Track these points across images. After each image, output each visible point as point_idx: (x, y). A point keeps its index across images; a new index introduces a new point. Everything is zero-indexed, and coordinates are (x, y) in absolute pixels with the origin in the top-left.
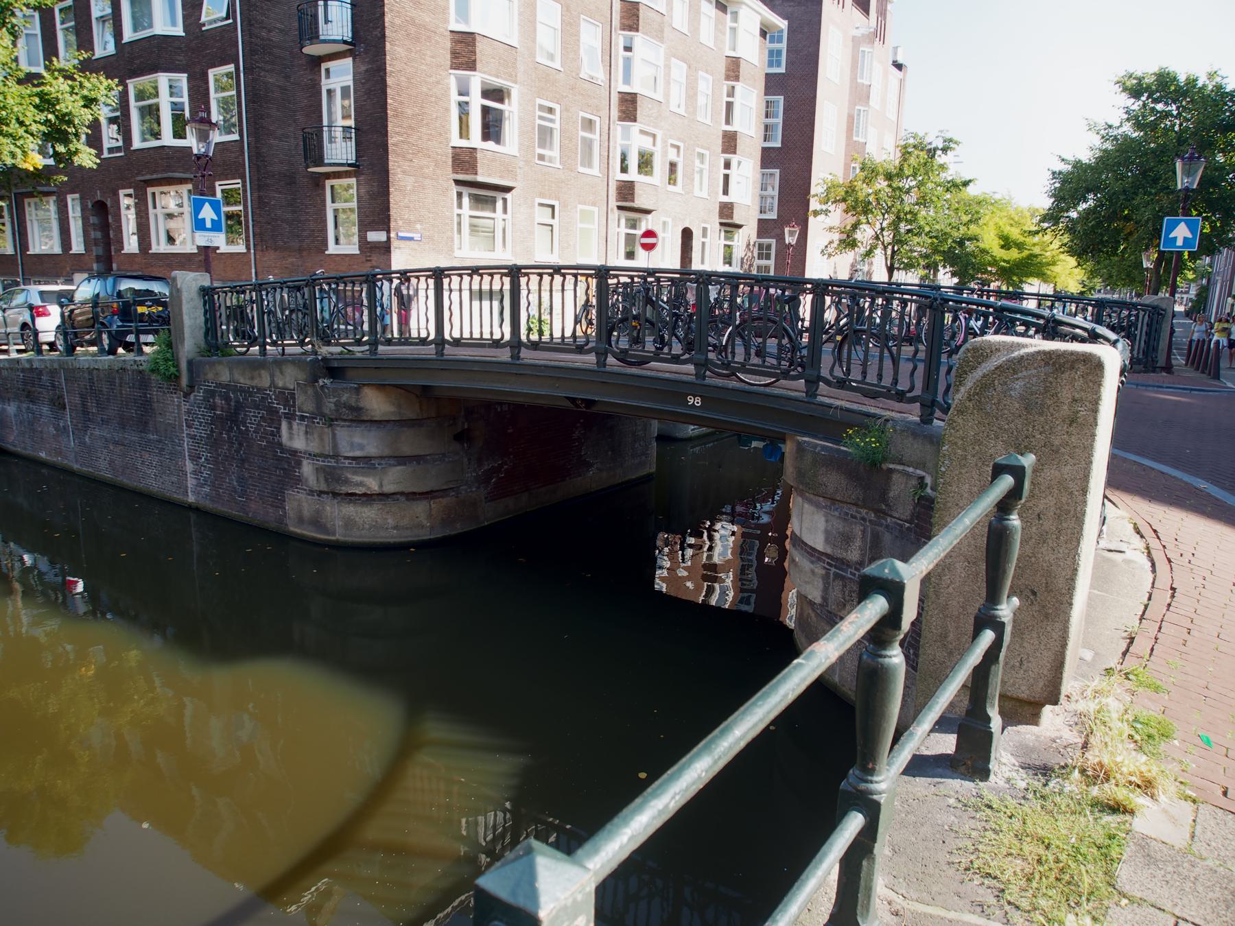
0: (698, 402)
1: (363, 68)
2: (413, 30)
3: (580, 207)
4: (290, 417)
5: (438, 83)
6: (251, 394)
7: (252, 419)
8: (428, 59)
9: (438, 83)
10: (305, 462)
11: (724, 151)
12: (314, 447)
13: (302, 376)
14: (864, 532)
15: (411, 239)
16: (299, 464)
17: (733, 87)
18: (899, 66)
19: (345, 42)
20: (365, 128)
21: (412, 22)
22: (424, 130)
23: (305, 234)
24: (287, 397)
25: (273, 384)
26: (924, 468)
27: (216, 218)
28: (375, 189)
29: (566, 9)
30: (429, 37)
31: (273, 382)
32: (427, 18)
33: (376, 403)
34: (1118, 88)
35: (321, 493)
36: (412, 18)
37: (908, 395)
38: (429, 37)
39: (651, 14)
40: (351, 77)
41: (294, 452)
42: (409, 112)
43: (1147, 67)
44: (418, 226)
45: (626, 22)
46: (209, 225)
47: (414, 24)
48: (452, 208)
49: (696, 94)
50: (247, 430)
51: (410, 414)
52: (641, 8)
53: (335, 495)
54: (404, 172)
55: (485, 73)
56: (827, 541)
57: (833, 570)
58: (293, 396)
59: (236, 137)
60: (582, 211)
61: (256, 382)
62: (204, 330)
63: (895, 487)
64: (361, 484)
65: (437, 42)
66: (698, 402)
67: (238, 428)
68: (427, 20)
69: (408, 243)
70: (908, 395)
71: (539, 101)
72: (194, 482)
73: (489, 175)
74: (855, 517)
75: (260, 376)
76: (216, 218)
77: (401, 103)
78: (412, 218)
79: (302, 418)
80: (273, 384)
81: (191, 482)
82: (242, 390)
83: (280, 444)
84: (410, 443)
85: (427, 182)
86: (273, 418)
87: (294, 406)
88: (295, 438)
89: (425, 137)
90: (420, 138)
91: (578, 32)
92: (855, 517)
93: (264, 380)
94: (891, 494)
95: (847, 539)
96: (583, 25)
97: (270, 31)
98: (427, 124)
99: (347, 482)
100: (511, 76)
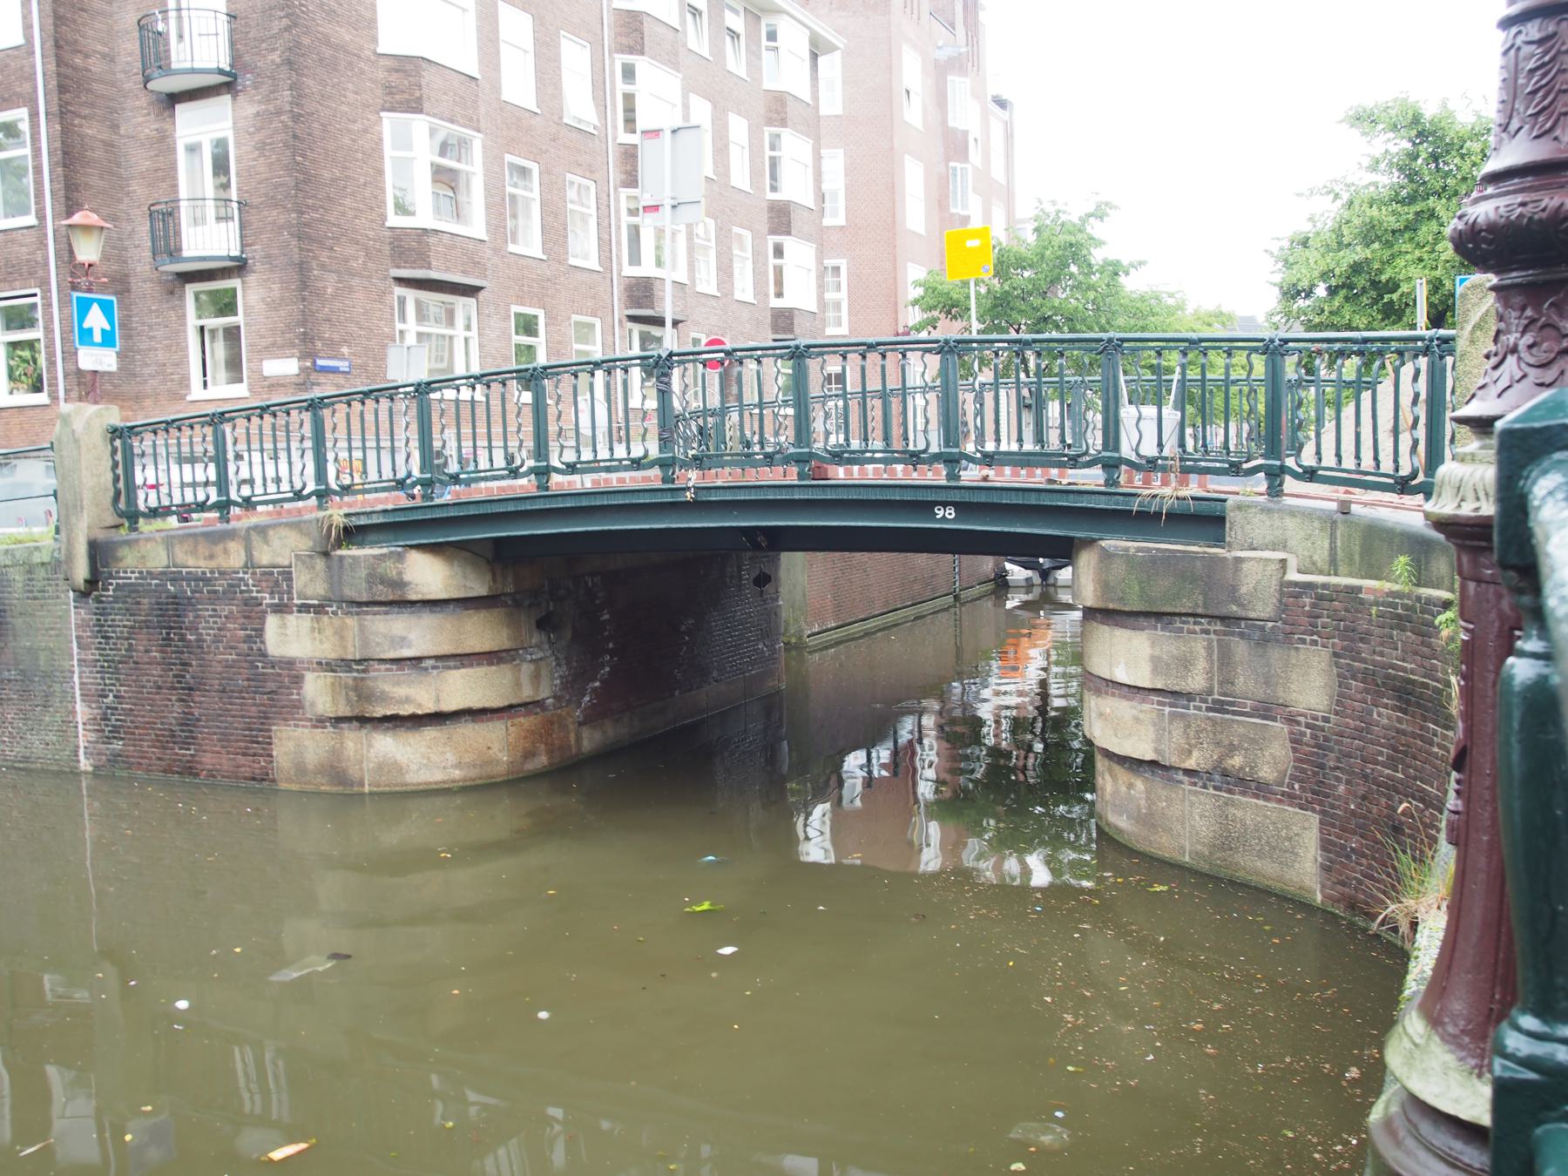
0: (950, 513)
1: (251, 110)
2: (328, 52)
3: (575, 317)
4: (281, 609)
5: (365, 131)
6: (207, 581)
7: (208, 623)
8: (351, 96)
9: (365, 131)
10: (309, 677)
11: (773, 232)
12: (327, 649)
13: (303, 544)
14: (1209, 648)
15: (335, 370)
16: (298, 680)
17: (778, 136)
18: (1001, 103)
19: (221, 72)
20: (256, 201)
21: (326, 41)
22: (348, 202)
23: (147, 371)
24: (279, 579)
25: (250, 564)
26: (1285, 548)
27: (108, 328)
28: (276, 294)
29: (539, 23)
30: (350, 63)
31: (249, 555)
32: (345, 35)
33: (428, 574)
34: (1345, 126)
35: (339, 720)
36: (326, 36)
37: (1245, 466)
38: (350, 63)
39: (660, 30)
40: (229, 124)
41: (290, 663)
42: (327, 175)
43: (1379, 94)
44: (345, 350)
45: (625, 41)
46: (97, 338)
47: (328, 43)
48: (393, 321)
49: (727, 146)
50: (200, 640)
51: (479, 589)
52: (646, 20)
53: (363, 720)
54: (323, 267)
55: (434, 116)
56: (1155, 670)
57: (1167, 709)
58: (288, 576)
59: (31, 220)
60: (576, 323)
61: (222, 562)
62: (111, 493)
63: (1249, 580)
64: (408, 700)
65: (362, 72)
66: (950, 513)
67: (183, 638)
68: (348, 38)
69: (331, 376)
70: (1245, 466)
71: (509, 158)
72: (93, 736)
73: (447, 270)
74: (1194, 632)
75: (226, 551)
76: (108, 328)
77: (313, 161)
78: (336, 337)
79: (305, 608)
80: (250, 564)
81: (83, 738)
82: (193, 578)
83: (263, 654)
84: (480, 632)
85: (355, 282)
86: (253, 615)
87: (290, 592)
88: (289, 638)
89: (350, 214)
90: (343, 214)
91: (559, 54)
92: (1194, 632)
93: (234, 557)
94: (1244, 590)
95: (1185, 663)
96: (564, 42)
97: (87, 56)
98: (353, 194)
99: (384, 698)
100: (471, 120)
